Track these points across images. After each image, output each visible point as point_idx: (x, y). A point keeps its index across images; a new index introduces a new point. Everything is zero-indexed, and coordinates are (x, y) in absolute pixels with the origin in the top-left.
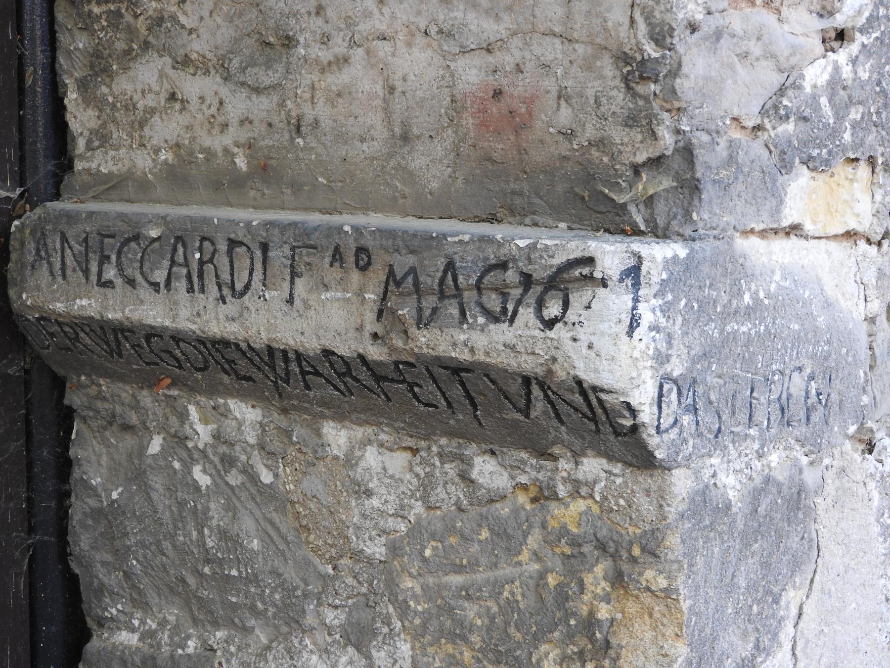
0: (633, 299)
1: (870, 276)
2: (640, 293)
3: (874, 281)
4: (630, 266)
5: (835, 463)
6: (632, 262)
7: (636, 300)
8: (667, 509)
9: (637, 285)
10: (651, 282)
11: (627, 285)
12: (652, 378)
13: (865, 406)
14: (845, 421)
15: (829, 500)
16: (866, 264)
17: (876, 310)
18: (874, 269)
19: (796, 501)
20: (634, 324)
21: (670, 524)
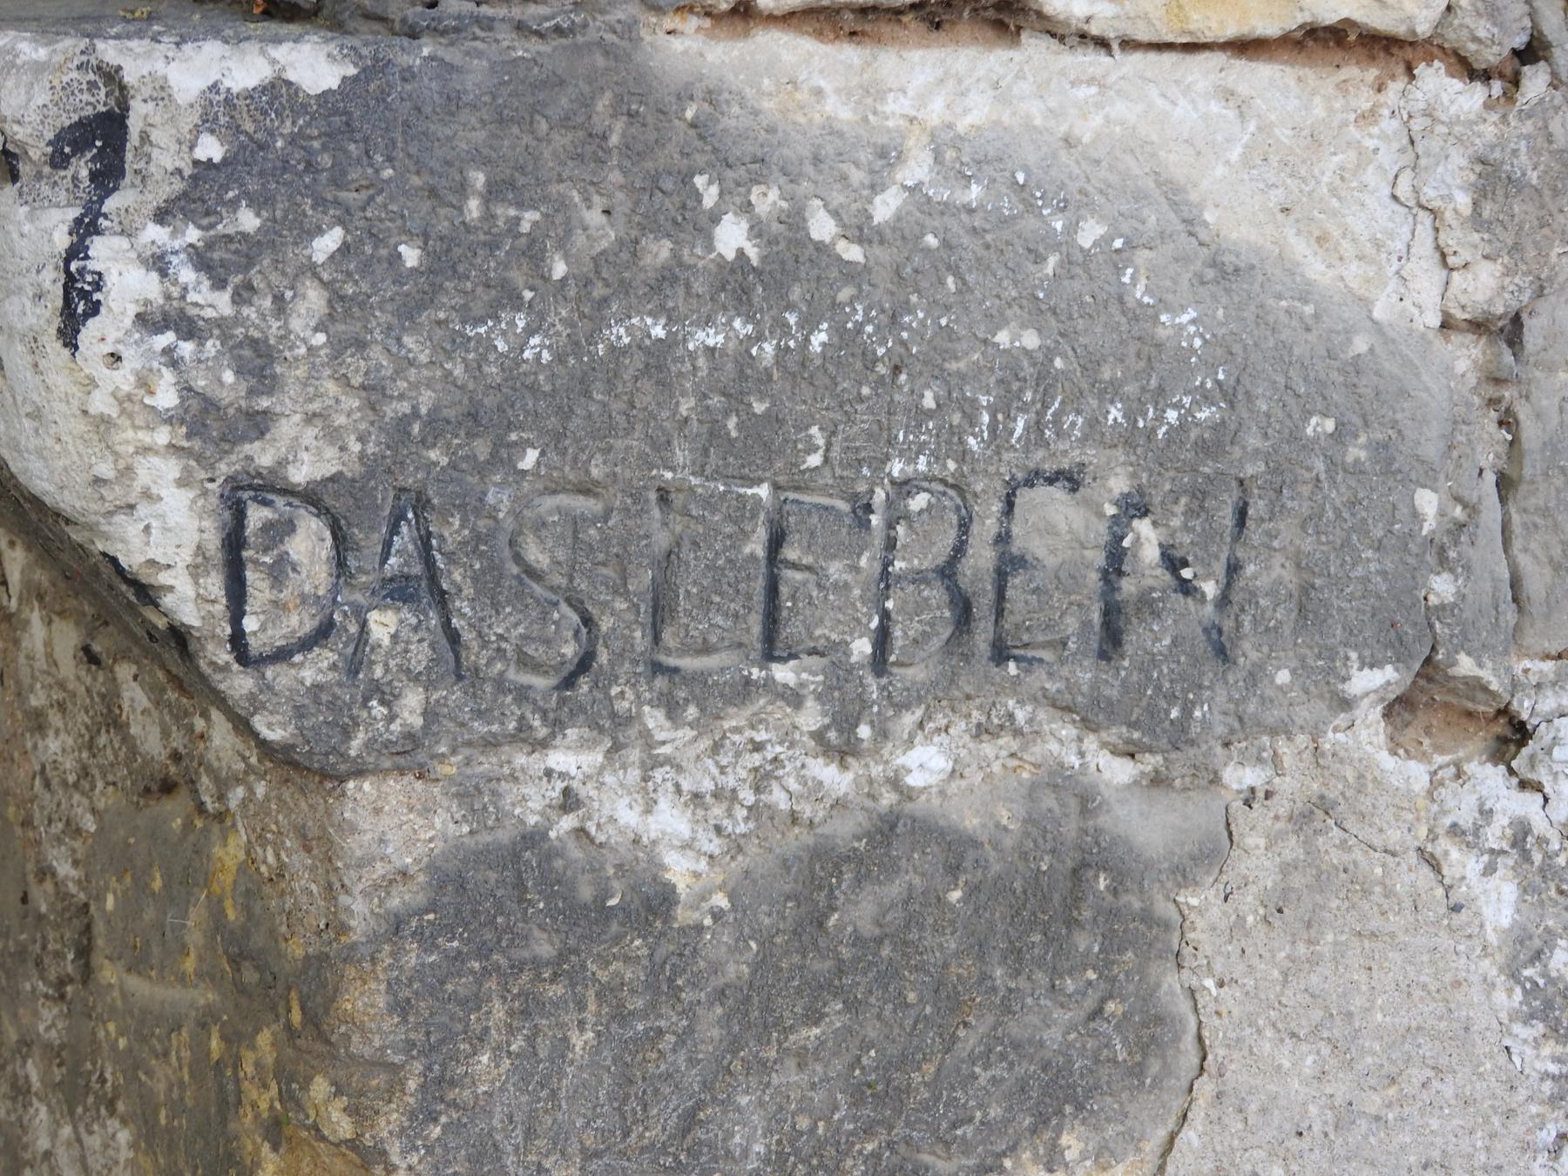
0: (78, 221)
1: (1451, 186)
2: (110, 204)
3: (1463, 201)
4: (89, 111)
5: (1285, 785)
6: (101, 101)
7: (86, 228)
8: (344, 899)
9: (108, 176)
10: (152, 169)
11: (75, 178)
12: (182, 483)
13: (1443, 607)
14: (1330, 654)
15: (1247, 901)
16: (1435, 144)
17: (1480, 297)
18: (1458, 159)
19: (1068, 903)
20: (79, 302)
21: (353, 947)
